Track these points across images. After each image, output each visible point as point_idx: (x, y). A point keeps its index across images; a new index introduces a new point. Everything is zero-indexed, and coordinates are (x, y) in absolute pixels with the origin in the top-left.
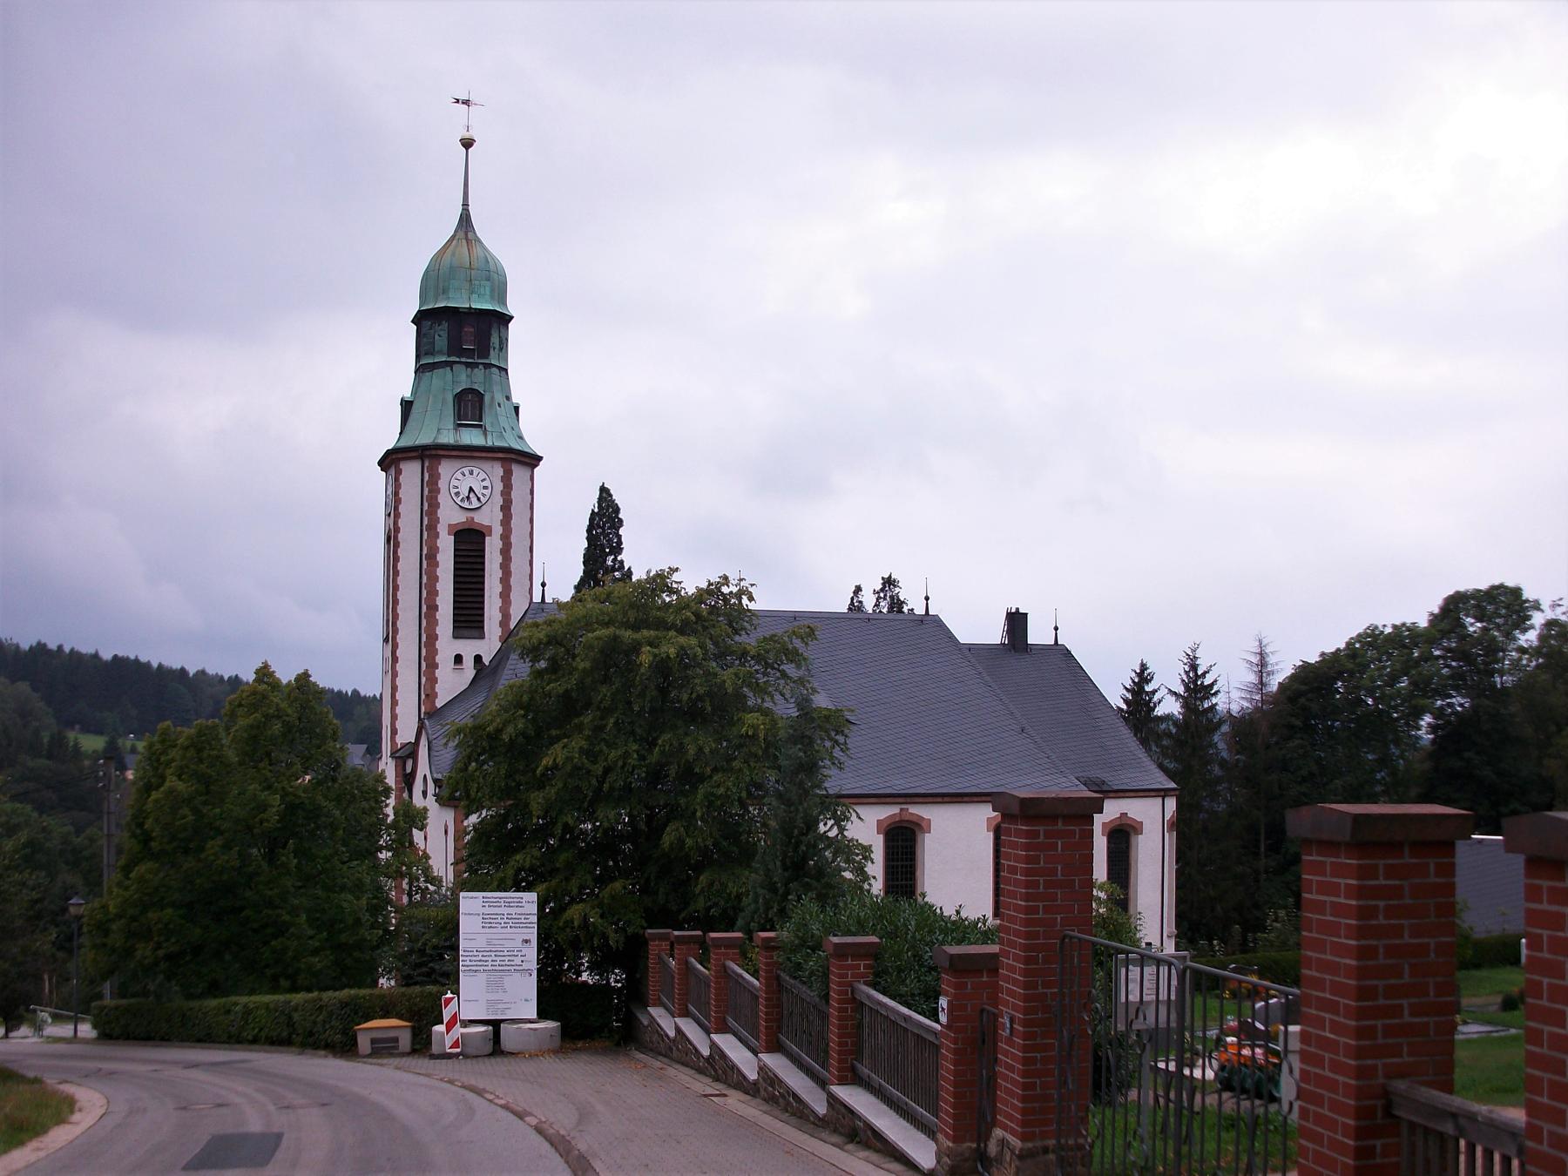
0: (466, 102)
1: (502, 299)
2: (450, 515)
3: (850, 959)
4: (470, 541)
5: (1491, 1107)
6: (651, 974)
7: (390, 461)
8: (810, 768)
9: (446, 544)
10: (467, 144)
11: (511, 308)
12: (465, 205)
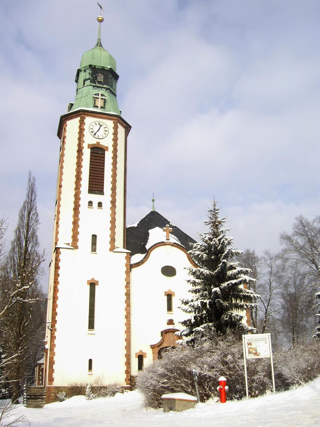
2: (89, 140)
3: (243, 301)
5: (47, 326)
6: (35, 386)
8: (43, 320)
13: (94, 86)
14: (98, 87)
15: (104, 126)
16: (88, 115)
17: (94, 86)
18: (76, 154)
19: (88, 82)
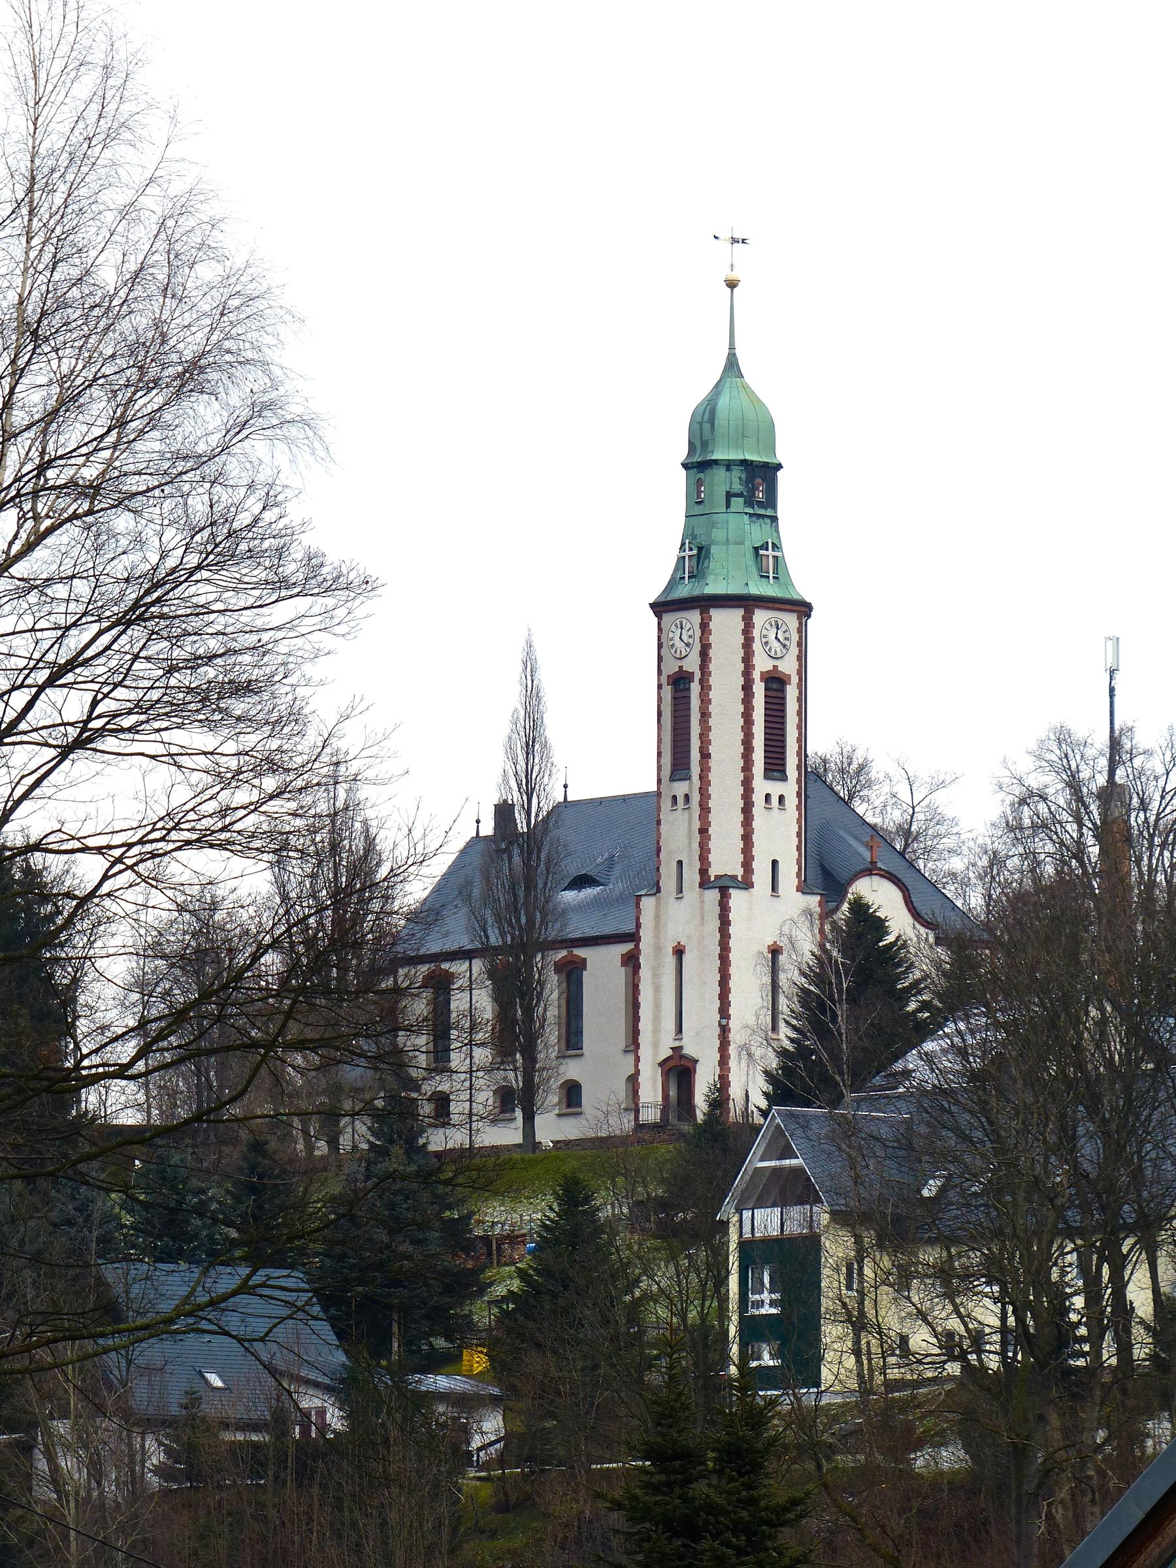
0: (734, 241)
1: (772, 449)
4: (776, 683)
7: (660, 608)
9: (759, 689)
10: (732, 285)
11: (781, 457)
12: (732, 348)
13: (751, 515)
15: (784, 628)
16: (758, 607)
17: (751, 515)
18: (741, 695)
19: (738, 503)
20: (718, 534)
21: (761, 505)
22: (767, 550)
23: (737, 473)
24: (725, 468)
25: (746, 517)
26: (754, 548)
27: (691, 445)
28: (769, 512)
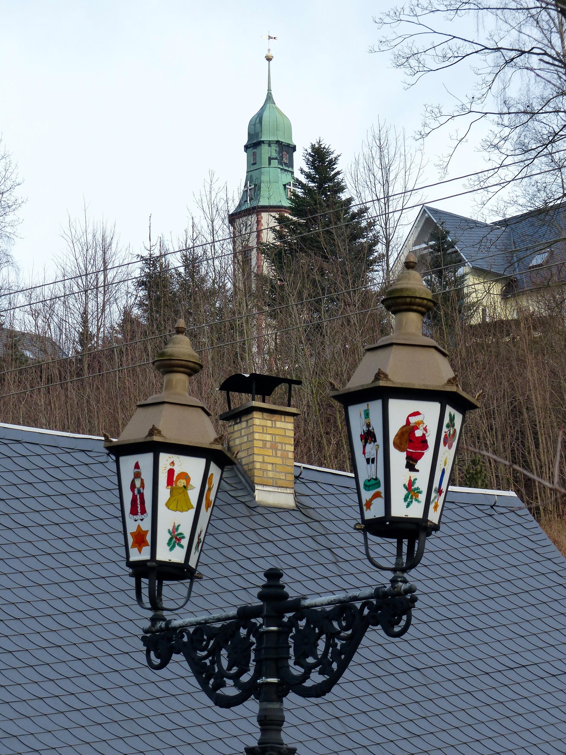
0: (270, 38)
10: (269, 59)
12: (269, 90)
13: (282, 169)
14: (286, 170)
17: (282, 169)
20: (264, 178)
21: (286, 164)
22: (290, 186)
23: (274, 147)
24: (268, 145)
25: (279, 170)
26: (283, 185)
27: (249, 135)
28: (290, 169)
